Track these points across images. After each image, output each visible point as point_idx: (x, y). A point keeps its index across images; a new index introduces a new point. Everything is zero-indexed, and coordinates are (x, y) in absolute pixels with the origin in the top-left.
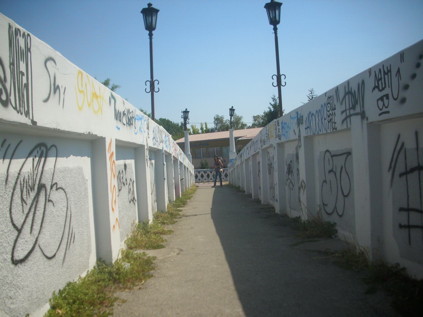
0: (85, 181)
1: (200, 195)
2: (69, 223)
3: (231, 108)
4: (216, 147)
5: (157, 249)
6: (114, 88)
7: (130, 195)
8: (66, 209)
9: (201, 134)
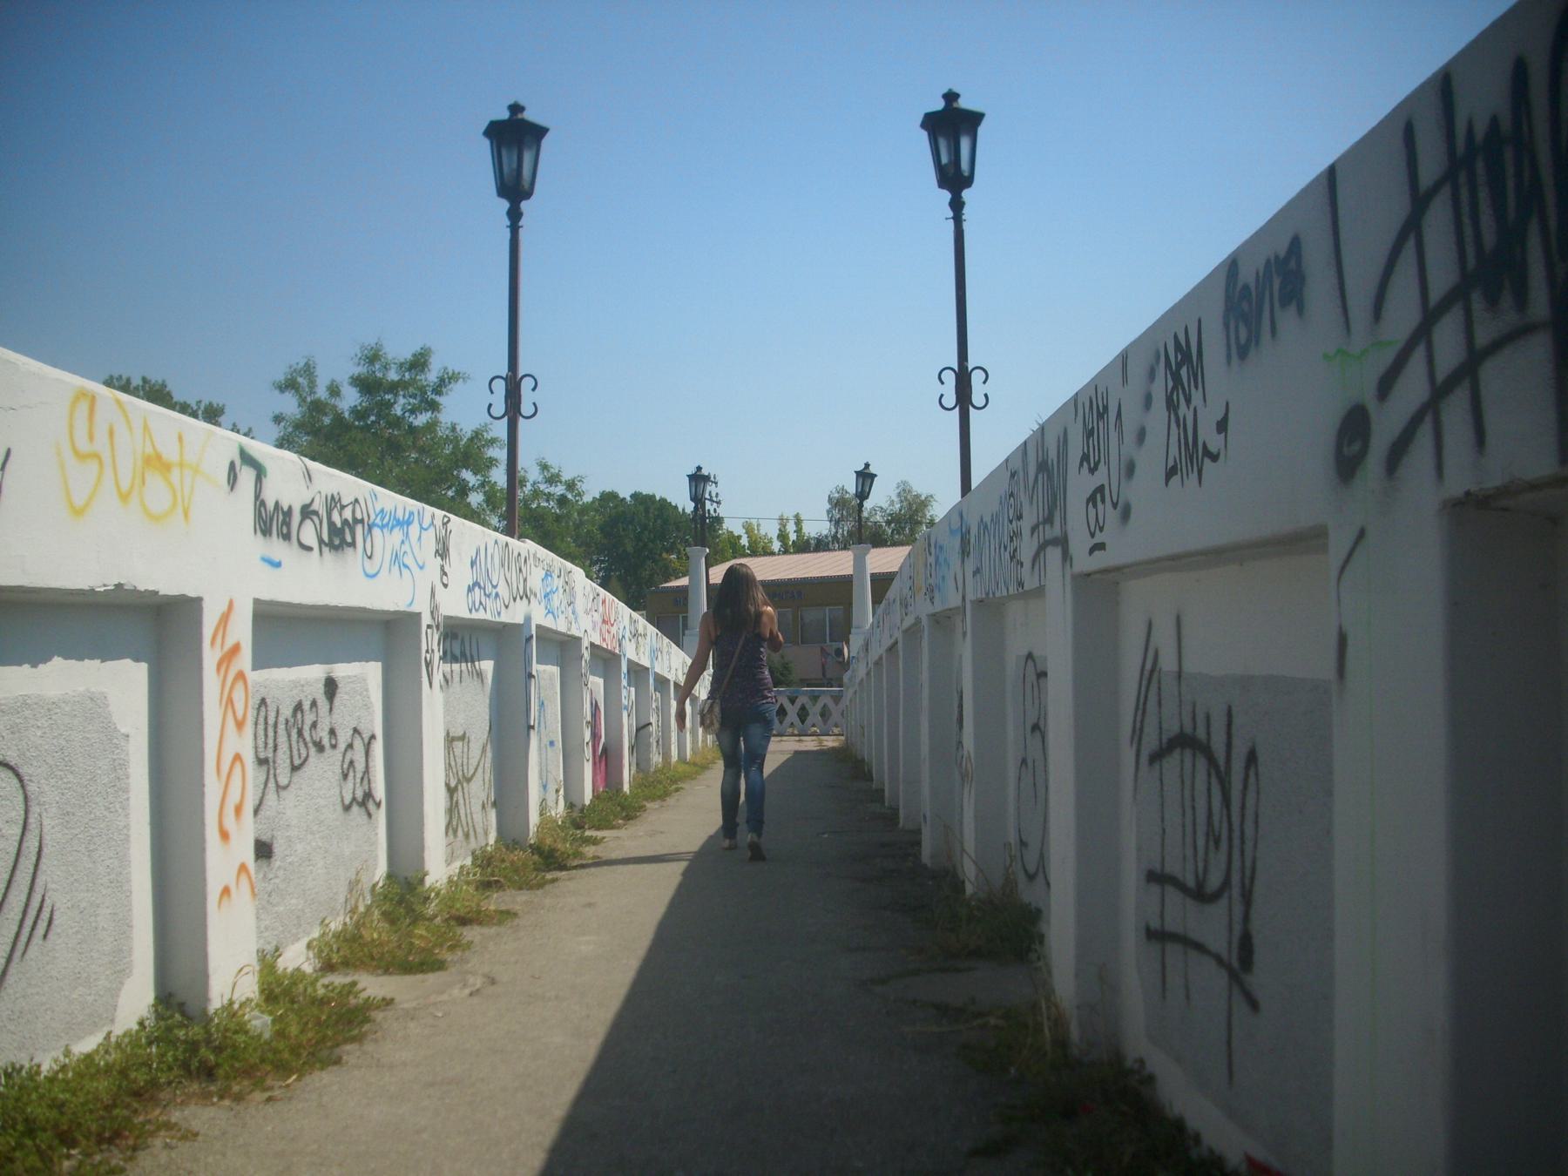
0: (115, 741)
1: (708, 786)
3: (861, 467)
5: (415, 973)
6: (447, 380)
7: (350, 784)
8: (18, 831)
9: (779, 554)
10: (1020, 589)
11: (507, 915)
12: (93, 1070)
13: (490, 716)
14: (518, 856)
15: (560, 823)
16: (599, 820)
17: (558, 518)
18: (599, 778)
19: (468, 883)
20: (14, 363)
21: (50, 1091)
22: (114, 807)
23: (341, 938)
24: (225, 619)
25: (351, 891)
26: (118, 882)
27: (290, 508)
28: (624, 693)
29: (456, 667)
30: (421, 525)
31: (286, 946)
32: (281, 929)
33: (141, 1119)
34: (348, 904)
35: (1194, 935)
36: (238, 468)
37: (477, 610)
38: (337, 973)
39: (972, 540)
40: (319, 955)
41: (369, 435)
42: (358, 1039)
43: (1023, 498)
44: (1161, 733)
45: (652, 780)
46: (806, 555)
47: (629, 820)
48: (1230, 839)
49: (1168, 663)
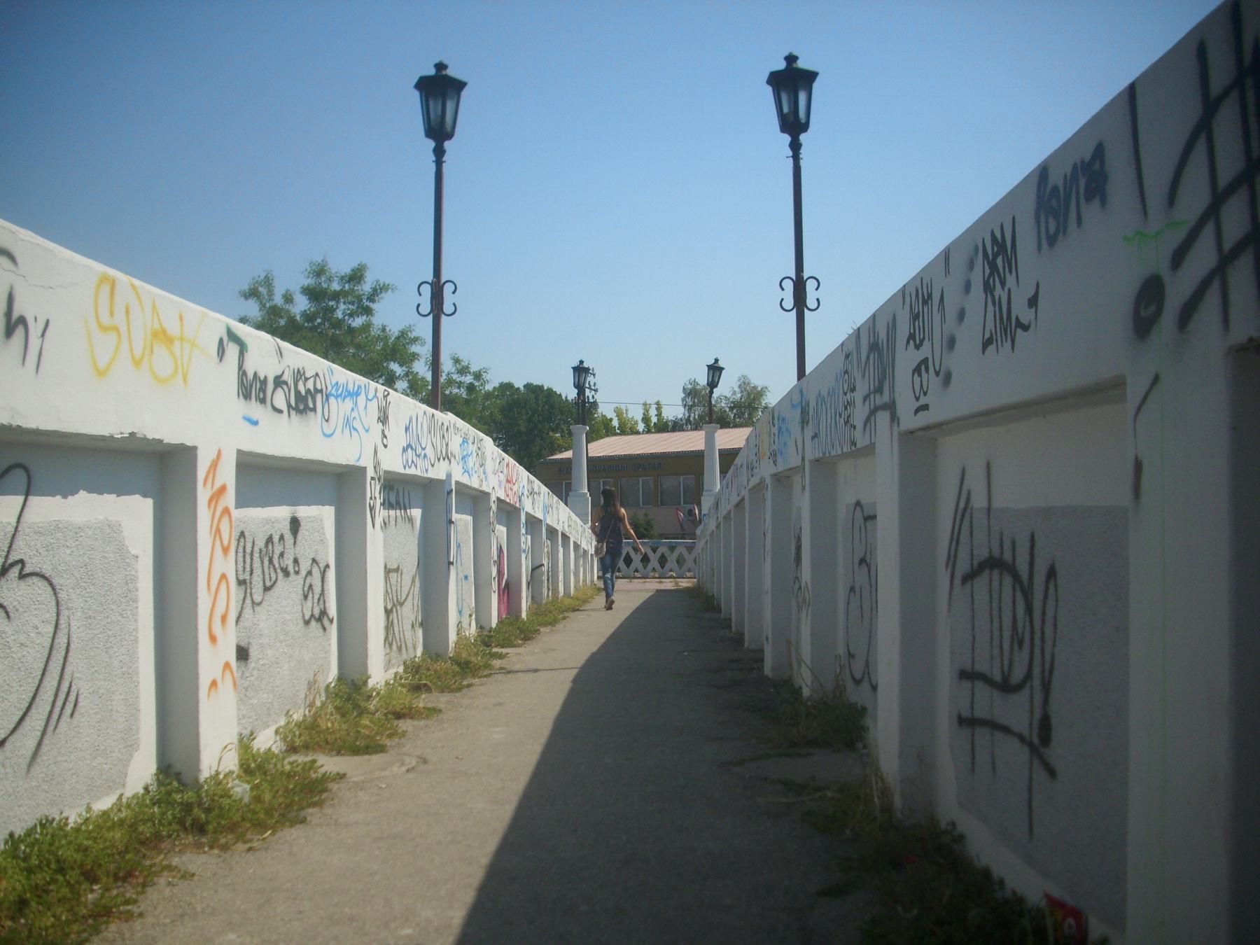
0: (127, 560)
2: (61, 665)
4: (604, 478)
5: (362, 754)
6: (379, 291)
7: (309, 604)
8: (51, 629)
9: (643, 433)
10: (853, 448)
11: (434, 711)
12: (109, 824)
13: (418, 554)
14: (440, 665)
15: (473, 641)
16: (503, 640)
17: (467, 402)
18: (502, 607)
19: (403, 686)
20: (52, 251)
21: (76, 838)
22: (126, 613)
23: (302, 726)
24: (215, 465)
25: (310, 689)
26: (129, 674)
27: (266, 377)
28: (523, 539)
29: (392, 513)
30: (367, 397)
31: (259, 731)
32: (255, 717)
33: (148, 863)
34: (307, 699)
35: (1001, 720)
36: (225, 343)
37: (410, 467)
38: (299, 754)
39: (811, 412)
40: (284, 739)
41: (316, 334)
42: (319, 804)
43: (857, 374)
44: (972, 559)
45: (544, 610)
46: (665, 434)
47: (526, 640)
48: (1032, 639)
49: (979, 502)
